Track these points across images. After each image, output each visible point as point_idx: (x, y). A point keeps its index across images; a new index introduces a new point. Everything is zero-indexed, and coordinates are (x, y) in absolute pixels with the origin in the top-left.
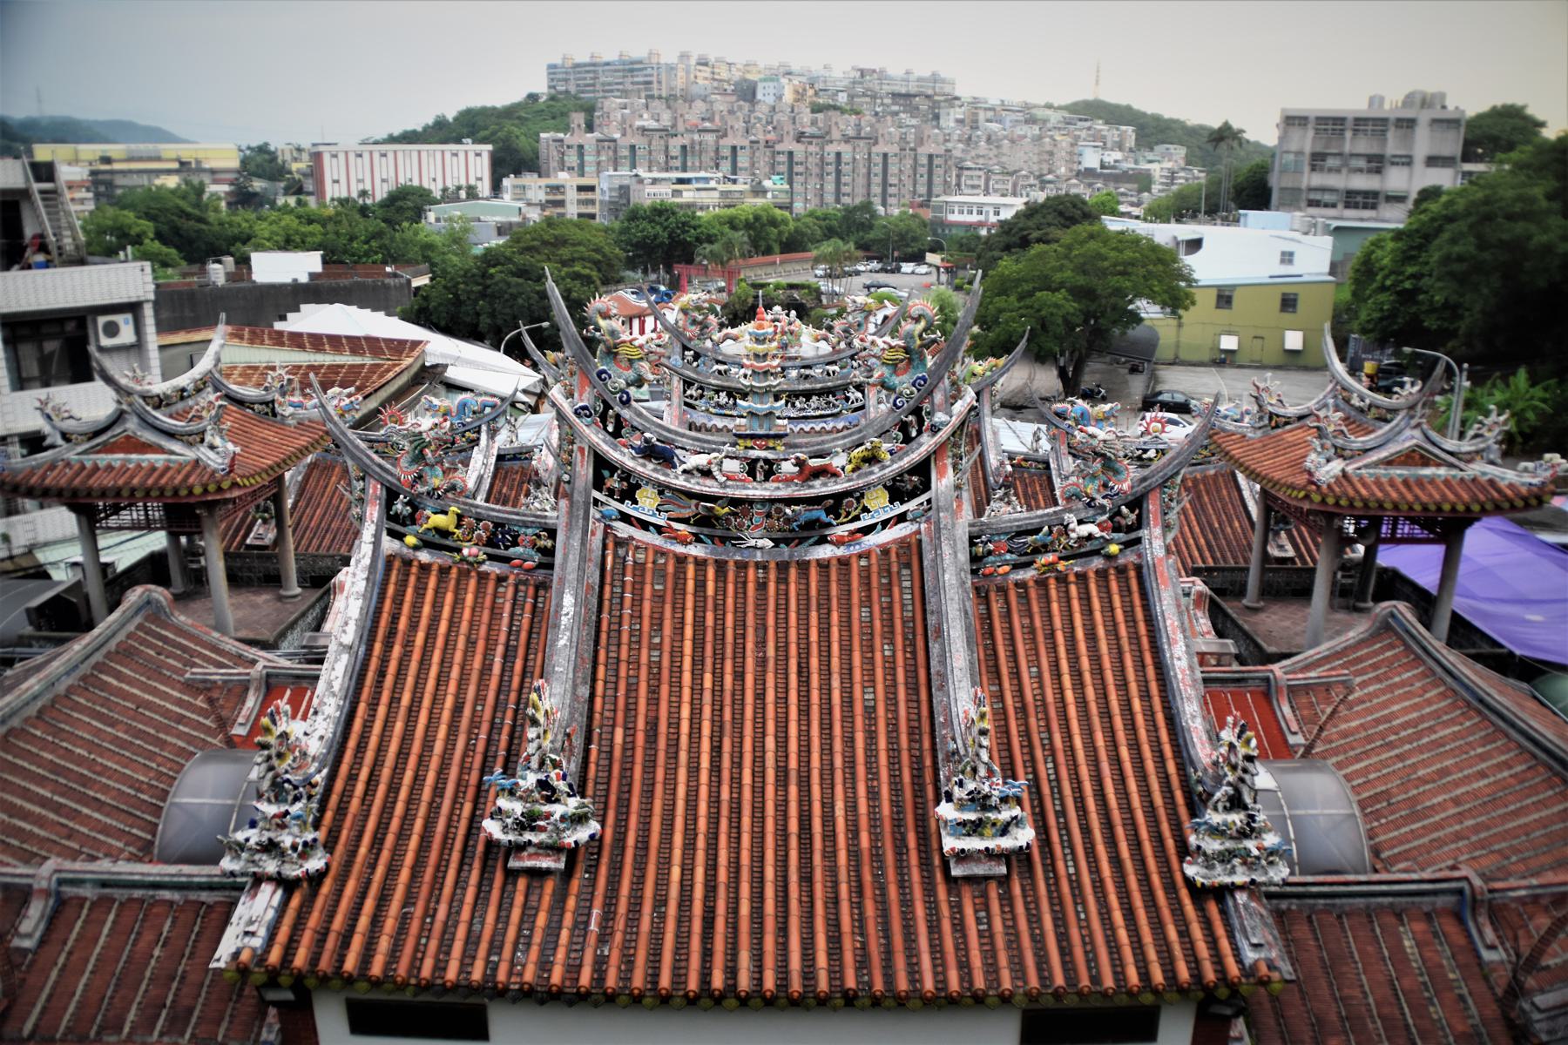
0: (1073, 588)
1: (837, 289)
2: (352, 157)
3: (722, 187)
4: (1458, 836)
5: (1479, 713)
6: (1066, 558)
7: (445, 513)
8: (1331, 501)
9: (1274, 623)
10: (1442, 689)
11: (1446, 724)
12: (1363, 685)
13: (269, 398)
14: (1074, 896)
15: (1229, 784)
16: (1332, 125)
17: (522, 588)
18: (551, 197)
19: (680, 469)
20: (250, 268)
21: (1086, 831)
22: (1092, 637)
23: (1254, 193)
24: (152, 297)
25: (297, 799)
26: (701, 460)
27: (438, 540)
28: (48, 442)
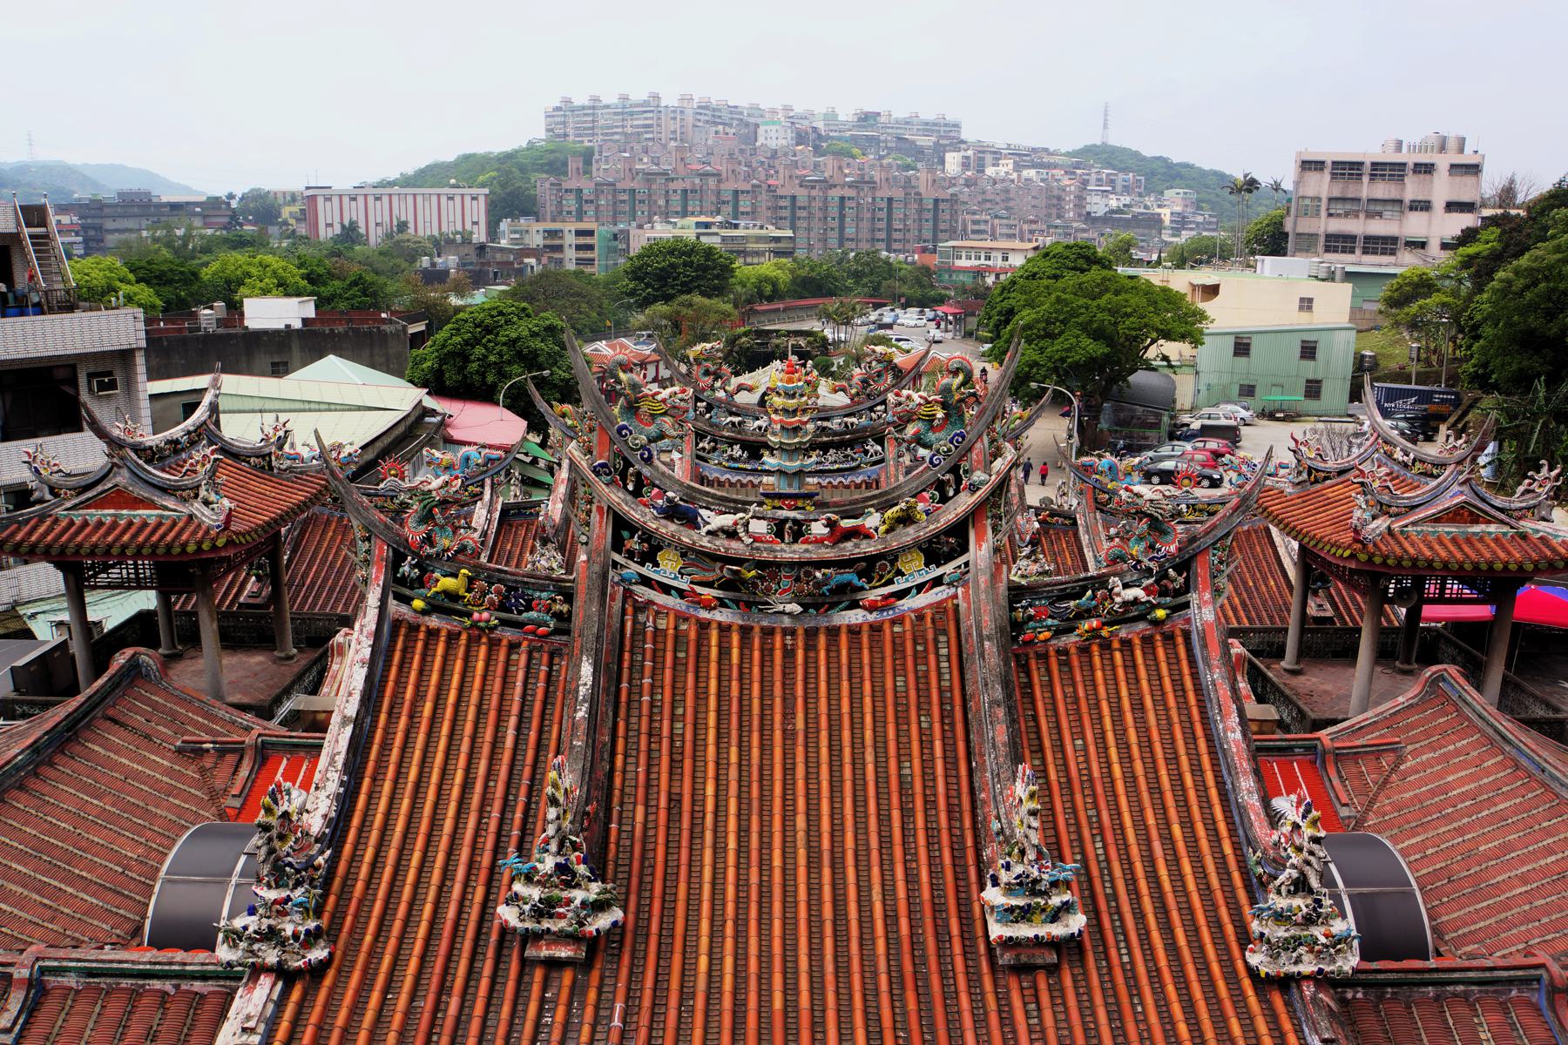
0: (1118, 655)
1: (843, 336)
2: (346, 200)
3: (724, 232)
4: (1527, 918)
5: (1543, 784)
6: (1111, 624)
7: (455, 576)
8: (1378, 560)
9: (1319, 683)
10: (1500, 758)
11: (1508, 796)
12: (1416, 753)
13: (267, 450)
14: (1128, 987)
15: (1293, 866)
16: (1347, 170)
17: (536, 655)
18: (548, 242)
19: (704, 530)
20: (242, 314)
21: (1140, 916)
22: (1138, 706)
23: (1274, 242)
24: (143, 344)
25: (298, 884)
26: (727, 520)
27: (448, 604)
28: (36, 495)
